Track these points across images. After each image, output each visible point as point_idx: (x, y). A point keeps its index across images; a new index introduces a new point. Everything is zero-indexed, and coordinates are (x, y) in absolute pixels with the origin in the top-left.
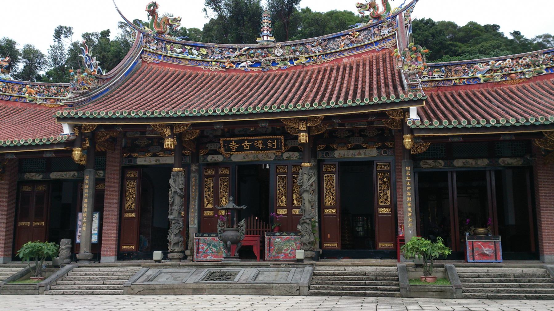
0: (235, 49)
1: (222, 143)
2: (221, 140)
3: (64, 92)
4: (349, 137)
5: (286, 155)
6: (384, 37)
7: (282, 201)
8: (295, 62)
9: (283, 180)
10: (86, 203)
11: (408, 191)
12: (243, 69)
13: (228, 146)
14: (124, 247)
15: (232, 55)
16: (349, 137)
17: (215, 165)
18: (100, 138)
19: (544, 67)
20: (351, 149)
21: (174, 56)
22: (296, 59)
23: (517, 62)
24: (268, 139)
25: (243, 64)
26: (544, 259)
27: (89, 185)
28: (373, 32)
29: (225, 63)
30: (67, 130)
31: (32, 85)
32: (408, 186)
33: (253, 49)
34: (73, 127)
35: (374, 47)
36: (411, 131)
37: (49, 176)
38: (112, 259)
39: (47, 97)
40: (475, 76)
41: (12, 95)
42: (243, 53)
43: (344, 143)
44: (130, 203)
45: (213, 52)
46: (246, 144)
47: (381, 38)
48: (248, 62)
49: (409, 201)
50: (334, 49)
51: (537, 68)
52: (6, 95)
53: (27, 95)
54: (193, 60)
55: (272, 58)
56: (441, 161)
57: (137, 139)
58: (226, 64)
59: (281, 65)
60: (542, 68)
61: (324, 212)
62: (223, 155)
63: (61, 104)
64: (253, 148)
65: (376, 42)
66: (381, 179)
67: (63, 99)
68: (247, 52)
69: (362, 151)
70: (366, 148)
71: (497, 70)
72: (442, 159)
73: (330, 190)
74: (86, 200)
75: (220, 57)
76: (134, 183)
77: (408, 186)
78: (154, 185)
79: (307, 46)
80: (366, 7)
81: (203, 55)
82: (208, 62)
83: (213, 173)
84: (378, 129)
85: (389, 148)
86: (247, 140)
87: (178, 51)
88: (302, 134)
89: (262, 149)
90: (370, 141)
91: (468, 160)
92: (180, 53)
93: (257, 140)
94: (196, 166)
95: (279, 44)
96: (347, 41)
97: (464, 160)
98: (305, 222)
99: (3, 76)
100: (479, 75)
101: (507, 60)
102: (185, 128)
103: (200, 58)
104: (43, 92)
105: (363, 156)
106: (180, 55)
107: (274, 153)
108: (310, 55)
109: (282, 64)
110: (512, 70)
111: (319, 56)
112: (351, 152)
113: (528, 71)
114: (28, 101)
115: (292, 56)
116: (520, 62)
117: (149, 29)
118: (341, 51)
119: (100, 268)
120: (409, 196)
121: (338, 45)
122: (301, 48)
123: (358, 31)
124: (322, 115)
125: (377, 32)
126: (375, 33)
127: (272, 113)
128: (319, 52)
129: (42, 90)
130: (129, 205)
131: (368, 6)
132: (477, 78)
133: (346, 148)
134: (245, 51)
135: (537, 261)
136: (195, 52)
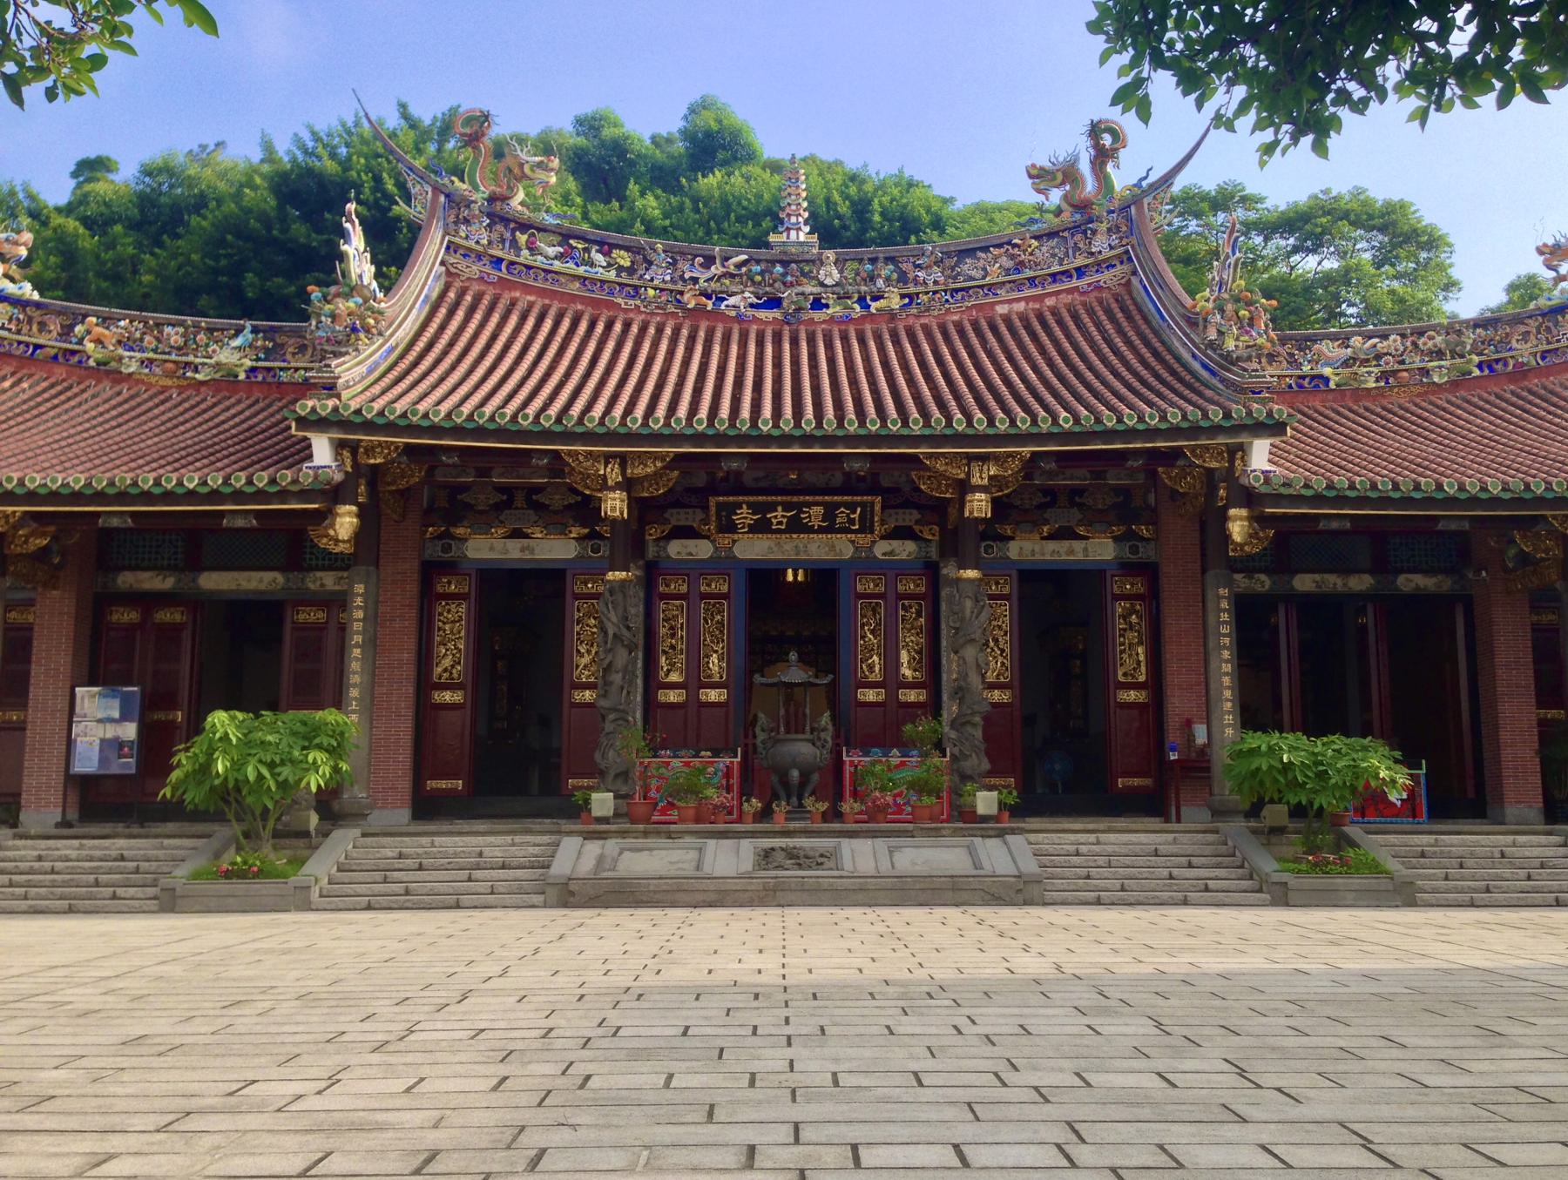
0: (709, 261)
1: (713, 510)
2: (713, 501)
3: (207, 345)
4: (1042, 507)
5: (881, 549)
6: (1100, 258)
7: (871, 668)
8: (874, 306)
9: (874, 611)
10: (357, 659)
11: (1225, 647)
12: (733, 313)
13: (729, 517)
14: (431, 784)
15: (703, 276)
16: (1042, 507)
17: (694, 570)
18: (393, 482)
19: (1476, 359)
20: (1051, 537)
21: (538, 264)
22: (875, 299)
23: (1414, 344)
24: (838, 505)
25: (732, 301)
26: (1503, 815)
27: (365, 609)
28: (1071, 243)
29: (682, 293)
30: (322, 451)
31: (105, 319)
32: (1225, 635)
33: (758, 262)
34: (339, 446)
35: (1075, 283)
36: (1249, 497)
37: (1289, 582)
38: (1533, 809)
39: (151, 355)
40: (1315, 372)
41: (41, 341)
42: (732, 269)
43: (485, 520)
44: (447, 662)
45: (650, 263)
46: (779, 516)
47: (1091, 260)
48: (747, 294)
49: (1227, 674)
50: (972, 279)
51: (1458, 360)
52: (20, 343)
53: (90, 346)
54: (594, 281)
55: (810, 288)
56: (1263, 577)
57: (465, 488)
58: (686, 297)
59: (835, 310)
60: (1470, 362)
61: (1014, 696)
62: (713, 542)
63: (199, 377)
64: (796, 526)
65: (1080, 272)
66: (1125, 617)
67: (204, 364)
68: (744, 269)
69: (1078, 545)
70: (1087, 538)
71: (1367, 360)
72: (1371, 572)
73: (996, 641)
74: (357, 652)
75: (668, 278)
76: (461, 610)
77: (1225, 635)
78: (521, 617)
79: (904, 266)
80: (1054, 179)
81: (620, 269)
82: (636, 288)
83: (684, 589)
84: (1117, 490)
85: (1143, 539)
86: (783, 504)
87: (551, 251)
88: (978, 496)
89: (821, 530)
90: (1097, 519)
91: (1326, 576)
92: (556, 258)
93: (809, 505)
94: (638, 568)
95: (830, 255)
96: (1006, 262)
97: (1317, 577)
98: (968, 722)
99: (11, 288)
100: (1327, 371)
101: (1392, 337)
102: (659, 464)
103: (612, 275)
104: (142, 340)
105: (1081, 557)
106: (556, 262)
107: (853, 542)
108: (912, 290)
109: (838, 308)
110: (1402, 362)
111: (935, 293)
112: (1052, 546)
113: (1440, 367)
114: (92, 363)
115: (863, 288)
116: (1420, 342)
117: (465, 186)
118: (991, 287)
119: (85, 842)
120: (1227, 661)
121: (984, 269)
122: (887, 270)
123: (1035, 238)
124: (1027, 450)
125: (1081, 245)
126: (1076, 248)
127: (996, 436)
128: (936, 283)
129: (138, 335)
130: (445, 670)
131: (1060, 177)
132: (1321, 377)
133: (1037, 536)
134: (739, 266)
135: (1154, 823)
136: (599, 258)
